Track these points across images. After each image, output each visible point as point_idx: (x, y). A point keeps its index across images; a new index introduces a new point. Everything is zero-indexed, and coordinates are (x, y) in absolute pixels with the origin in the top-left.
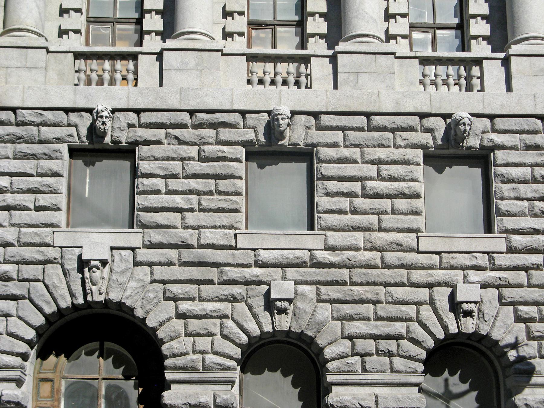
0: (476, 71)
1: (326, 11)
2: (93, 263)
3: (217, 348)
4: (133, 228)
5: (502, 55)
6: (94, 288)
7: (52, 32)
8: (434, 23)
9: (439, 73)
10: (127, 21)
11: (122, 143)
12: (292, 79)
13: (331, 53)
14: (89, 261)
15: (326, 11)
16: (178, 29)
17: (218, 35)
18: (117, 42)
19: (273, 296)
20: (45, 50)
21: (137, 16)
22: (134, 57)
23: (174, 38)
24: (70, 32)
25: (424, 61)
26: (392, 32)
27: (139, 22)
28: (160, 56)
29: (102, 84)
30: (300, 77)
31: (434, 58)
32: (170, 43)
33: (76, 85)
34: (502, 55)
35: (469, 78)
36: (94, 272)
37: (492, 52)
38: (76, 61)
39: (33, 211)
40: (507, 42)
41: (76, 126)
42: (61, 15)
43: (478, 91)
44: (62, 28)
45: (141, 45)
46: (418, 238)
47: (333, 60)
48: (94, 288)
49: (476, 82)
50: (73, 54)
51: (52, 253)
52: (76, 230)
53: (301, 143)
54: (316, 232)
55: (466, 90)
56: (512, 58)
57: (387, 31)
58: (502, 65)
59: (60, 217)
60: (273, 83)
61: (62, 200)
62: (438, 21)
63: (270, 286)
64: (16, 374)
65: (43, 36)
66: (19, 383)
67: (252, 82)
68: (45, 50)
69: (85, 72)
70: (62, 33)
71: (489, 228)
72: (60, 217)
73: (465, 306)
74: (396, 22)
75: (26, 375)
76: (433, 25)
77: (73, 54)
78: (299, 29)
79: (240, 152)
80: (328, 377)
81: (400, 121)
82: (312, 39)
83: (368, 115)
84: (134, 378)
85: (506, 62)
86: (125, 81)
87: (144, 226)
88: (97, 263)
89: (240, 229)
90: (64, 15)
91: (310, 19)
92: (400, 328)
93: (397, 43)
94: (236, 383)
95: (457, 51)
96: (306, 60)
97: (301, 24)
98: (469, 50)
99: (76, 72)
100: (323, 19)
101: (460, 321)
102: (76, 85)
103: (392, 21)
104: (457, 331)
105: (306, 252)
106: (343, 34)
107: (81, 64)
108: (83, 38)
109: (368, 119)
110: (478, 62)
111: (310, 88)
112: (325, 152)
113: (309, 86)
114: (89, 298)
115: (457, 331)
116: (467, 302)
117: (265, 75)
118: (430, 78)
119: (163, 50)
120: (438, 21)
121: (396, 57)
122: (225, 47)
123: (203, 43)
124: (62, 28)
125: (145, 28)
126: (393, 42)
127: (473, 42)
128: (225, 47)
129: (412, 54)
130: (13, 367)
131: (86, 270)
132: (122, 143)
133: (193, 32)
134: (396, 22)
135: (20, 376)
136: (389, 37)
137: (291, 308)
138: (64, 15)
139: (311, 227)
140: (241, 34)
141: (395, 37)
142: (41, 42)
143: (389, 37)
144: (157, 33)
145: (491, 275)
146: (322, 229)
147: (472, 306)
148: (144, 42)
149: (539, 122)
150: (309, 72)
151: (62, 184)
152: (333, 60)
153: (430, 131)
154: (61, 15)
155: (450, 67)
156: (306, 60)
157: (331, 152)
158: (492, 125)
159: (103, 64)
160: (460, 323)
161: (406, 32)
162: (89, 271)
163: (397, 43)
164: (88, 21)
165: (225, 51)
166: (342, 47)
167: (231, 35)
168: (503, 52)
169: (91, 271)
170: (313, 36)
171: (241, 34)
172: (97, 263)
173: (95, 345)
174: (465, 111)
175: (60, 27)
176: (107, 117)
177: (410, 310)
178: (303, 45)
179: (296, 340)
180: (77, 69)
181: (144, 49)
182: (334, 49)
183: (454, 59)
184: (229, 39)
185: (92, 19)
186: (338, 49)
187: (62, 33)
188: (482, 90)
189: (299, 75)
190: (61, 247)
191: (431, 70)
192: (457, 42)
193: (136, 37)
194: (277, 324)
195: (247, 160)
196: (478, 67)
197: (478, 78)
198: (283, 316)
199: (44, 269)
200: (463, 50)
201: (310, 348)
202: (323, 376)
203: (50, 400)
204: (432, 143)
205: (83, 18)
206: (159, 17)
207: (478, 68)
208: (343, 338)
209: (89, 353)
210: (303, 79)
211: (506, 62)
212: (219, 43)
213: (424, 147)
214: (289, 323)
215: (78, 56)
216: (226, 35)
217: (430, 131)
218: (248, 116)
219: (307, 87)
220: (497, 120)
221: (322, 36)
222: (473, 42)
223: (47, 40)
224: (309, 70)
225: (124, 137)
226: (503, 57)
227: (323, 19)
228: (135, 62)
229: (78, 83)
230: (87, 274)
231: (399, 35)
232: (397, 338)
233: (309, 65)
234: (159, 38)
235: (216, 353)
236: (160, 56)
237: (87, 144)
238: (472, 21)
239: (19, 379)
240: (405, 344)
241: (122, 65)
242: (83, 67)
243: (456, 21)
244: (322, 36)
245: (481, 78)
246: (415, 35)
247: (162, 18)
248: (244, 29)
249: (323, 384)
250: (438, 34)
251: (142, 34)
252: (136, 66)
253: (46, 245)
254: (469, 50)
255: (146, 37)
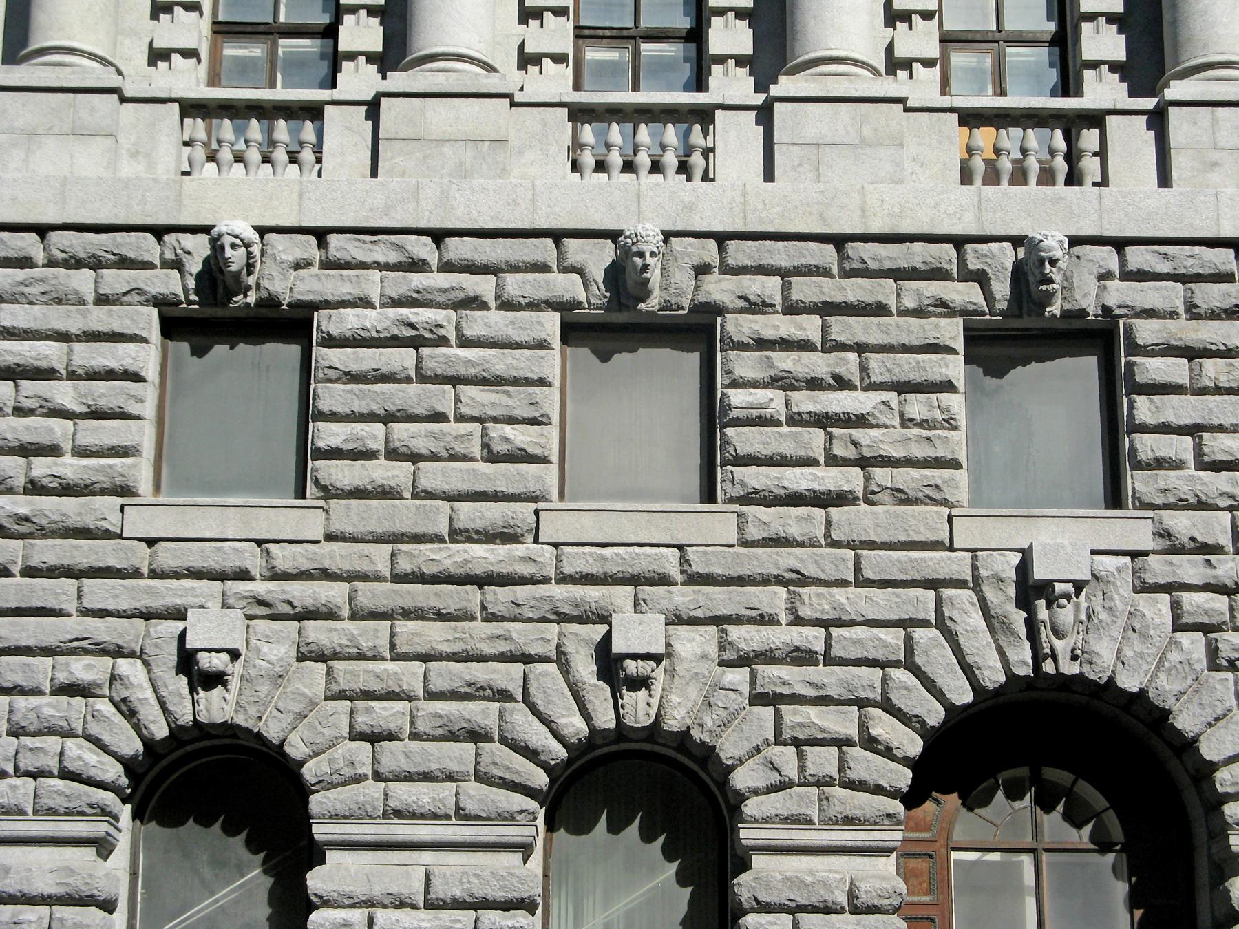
0: (1089, 139)
1: (1122, 11)
2: (1059, 587)
3: (855, 774)
4: (304, 496)
5: (1149, 103)
6: (1059, 644)
7: (134, 59)
8: (1000, 31)
9: (1005, 143)
10: (249, 29)
11: (1089, 315)
12: (670, 160)
13: (760, 99)
14: (1049, 584)
15: (1122, 11)
16: (798, 50)
17: (507, 61)
18: (642, 83)
19: (618, 647)
20: (115, 97)
21: (325, 19)
22: (314, 112)
23: (405, 69)
24: (544, 60)
25: (971, 118)
26: (900, 52)
27: (330, 32)
28: (373, 109)
29: (997, 182)
30: (689, 156)
31: (687, 109)
32: (398, 80)
33: (184, 173)
34: (1149, 103)
35: (1072, 157)
36: (1059, 606)
37: (1130, 96)
38: (186, 120)
39: (481, 462)
40: (1162, 72)
41: (580, 271)
42: (154, 16)
43: (1095, 184)
44: (156, 45)
45: (334, 85)
46: (950, 520)
47: (765, 115)
48: (1059, 644)
49: (1090, 166)
50: (566, 110)
51: (955, 565)
52: (1036, 512)
53: (1091, 310)
54: (307, 502)
55: (1066, 184)
56: (1172, 111)
57: (890, 49)
58: (1149, 128)
59: (958, 484)
60: (629, 167)
61: (143, 434)
62: (1009, 26)
63: (610, 625)
64: (99, 827)
65: (112, 64)
66: (104, 847)
67: (608, 167)
68: (115, 97)
69: (206, 145)
70: (157, 56)
71: (1115, 497)
72: (141, 472)
73: (631, 666)
74: (910, 28)
75: (120, 831)
76: (997, 36)
77: (566, 110)
78: (692, 47)
79: (551, 324)
80: (315, 829)
81: (919, 255)
82: (351, 64)
83: (839, 241)
84: (1118, 848)
85: (1158, 120)
86: (241, 165)
87: (328, 492)
88: (1069, 588)
89: (546, 501)
90: (162, 16)
91: (716, 21)
92: (483, 713)
93: (911, 77)
94: (536, 850)
95: (1053, 94)
96: (704, 115)
97: (696, 36)
98: (1079, 92)
99: (186, 144)
100: (745, 23)
101: (622, 699)
102: (184, 173)
103: (901, 27)
104: (613, 725)
105: (550, 548)
106: (788, 55)
107: (197, 128)
108: (203, 69)
109: (722, 249)
110: (1096, 119)
111: (713, 180)
112: (739, 326)
113: (711, 176)
114: (1048, 667)
115: (613, 725)
116: (635, 657)
117: (247, 147)
118: (1013, 156)
119: (380, 95)
120: (1009, 26)
121: (907, 110)
122: (522, 89)
123: (468, 77)
124: (156, 45)
125: (342, 47)
126: (902, 74)
127: (1088, 75)
128: (522, 89)
129: (946, 102)
130: (422, 816)
131: (1041, 603)
132: (1089, 315)
133: (837, 58)
134: (910, 28)
135: (108, 834)
136: (895, 64)
137: (236, 669)
138: (162, 16)
139: (709, 495)
140: (559, 59)
141: (907, 64)
142: (112, 80)
143: (895, 64)
144: (371, 58)
145: (683, 597)
146: (731, 501)
147: (645, 667)
148: (713, 82)
149: (1231, 253)
150: (710, 145)
151: (145, 399)
152: (765, 115)
153: (981, 278)
154: (154, 16)
155: (643, 127)
156: (704, 115)
157: (350, 321)
158: (1123, 262)
159: (299, 131)
160: (620, 701)
161: (933, 51)
162: (1048, 607)
163: (911, 77)
164: (577, 36)
165: (519, 98)
166: (784, 85)
167: (537, 60)
168: (1155, 97)
169: (1055, 606)
170: (721, 59)
171: (559, 59)
172: (1069, 588)
173: (1023, 772)
174: (1060, 231)
175: (521, 47)
176: (653, 254)
177: (508, 675)
178: (699, 82)
179: (674, 749)
180: (186, 139)
181: (336, 94)
182: (766, 90)
183: (234, 103)
184: (533, 69)
185: (586, 32)
186: (775, 90)
187: (157, 56)
188: (1103, 183)
189: (689, 150)
190: (556, 545)
191: (984, 137)
192: (1053, 76)
193: (324, 68)
194: (201, 707)
195: (565, 340)
196: (1097, 131)
197: (1095, 154)
198: (218, 691)
199: (79, 591)
200: (1066, 92)
201: (705, 769)
202: (732, 833)
203: (927, 899)
204: (582, 296)
205: (205, 25)
206: (375, 21)
207: (1095, 132)
208: (353, 738)
209: (1014, 793)
210: (697, 160)
211: (1158, 120)
212: (510, 78)
213: (160, 302)
214: (655, 709)
215: (191, 108)
216: (526, 60)
217: (981, 278)
218: (969, 247)
219: (706, 178)
220: (853, 249)
221: (741, 61)
222: (1088, 75)
223: (120, 73)
224: (710, 138)
225: (1088, 299)
226: (760, 102)
227: (745, 23)
228: (317, 123)
229: (188, 169)
230: (1043, 614)
231: (917, 60)
232: (476, 736)
233: (711, 127)
234: (373, 68)
235: (850, 785)
236: (373, 109)
237: (196, 306)
238: (1086, 27)
239: (104, 839)
240: (496, 752)
241: (651, 135)
242: (201, 135)
243: (684, 23)
244: (741, 61)
245: (1102, 154)
246: (593, 55)
247: (381, 25)
248: (933, 51)
249: (733, 848)
250: (646, 51)
251: (336, 60)
252: (320, 134)
253: (107, 535)
254: (1079, 92)
255: (346, 65)
